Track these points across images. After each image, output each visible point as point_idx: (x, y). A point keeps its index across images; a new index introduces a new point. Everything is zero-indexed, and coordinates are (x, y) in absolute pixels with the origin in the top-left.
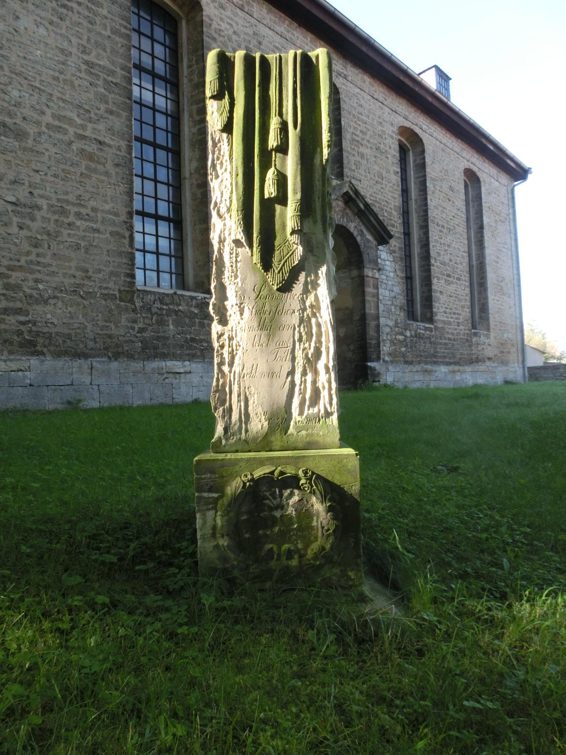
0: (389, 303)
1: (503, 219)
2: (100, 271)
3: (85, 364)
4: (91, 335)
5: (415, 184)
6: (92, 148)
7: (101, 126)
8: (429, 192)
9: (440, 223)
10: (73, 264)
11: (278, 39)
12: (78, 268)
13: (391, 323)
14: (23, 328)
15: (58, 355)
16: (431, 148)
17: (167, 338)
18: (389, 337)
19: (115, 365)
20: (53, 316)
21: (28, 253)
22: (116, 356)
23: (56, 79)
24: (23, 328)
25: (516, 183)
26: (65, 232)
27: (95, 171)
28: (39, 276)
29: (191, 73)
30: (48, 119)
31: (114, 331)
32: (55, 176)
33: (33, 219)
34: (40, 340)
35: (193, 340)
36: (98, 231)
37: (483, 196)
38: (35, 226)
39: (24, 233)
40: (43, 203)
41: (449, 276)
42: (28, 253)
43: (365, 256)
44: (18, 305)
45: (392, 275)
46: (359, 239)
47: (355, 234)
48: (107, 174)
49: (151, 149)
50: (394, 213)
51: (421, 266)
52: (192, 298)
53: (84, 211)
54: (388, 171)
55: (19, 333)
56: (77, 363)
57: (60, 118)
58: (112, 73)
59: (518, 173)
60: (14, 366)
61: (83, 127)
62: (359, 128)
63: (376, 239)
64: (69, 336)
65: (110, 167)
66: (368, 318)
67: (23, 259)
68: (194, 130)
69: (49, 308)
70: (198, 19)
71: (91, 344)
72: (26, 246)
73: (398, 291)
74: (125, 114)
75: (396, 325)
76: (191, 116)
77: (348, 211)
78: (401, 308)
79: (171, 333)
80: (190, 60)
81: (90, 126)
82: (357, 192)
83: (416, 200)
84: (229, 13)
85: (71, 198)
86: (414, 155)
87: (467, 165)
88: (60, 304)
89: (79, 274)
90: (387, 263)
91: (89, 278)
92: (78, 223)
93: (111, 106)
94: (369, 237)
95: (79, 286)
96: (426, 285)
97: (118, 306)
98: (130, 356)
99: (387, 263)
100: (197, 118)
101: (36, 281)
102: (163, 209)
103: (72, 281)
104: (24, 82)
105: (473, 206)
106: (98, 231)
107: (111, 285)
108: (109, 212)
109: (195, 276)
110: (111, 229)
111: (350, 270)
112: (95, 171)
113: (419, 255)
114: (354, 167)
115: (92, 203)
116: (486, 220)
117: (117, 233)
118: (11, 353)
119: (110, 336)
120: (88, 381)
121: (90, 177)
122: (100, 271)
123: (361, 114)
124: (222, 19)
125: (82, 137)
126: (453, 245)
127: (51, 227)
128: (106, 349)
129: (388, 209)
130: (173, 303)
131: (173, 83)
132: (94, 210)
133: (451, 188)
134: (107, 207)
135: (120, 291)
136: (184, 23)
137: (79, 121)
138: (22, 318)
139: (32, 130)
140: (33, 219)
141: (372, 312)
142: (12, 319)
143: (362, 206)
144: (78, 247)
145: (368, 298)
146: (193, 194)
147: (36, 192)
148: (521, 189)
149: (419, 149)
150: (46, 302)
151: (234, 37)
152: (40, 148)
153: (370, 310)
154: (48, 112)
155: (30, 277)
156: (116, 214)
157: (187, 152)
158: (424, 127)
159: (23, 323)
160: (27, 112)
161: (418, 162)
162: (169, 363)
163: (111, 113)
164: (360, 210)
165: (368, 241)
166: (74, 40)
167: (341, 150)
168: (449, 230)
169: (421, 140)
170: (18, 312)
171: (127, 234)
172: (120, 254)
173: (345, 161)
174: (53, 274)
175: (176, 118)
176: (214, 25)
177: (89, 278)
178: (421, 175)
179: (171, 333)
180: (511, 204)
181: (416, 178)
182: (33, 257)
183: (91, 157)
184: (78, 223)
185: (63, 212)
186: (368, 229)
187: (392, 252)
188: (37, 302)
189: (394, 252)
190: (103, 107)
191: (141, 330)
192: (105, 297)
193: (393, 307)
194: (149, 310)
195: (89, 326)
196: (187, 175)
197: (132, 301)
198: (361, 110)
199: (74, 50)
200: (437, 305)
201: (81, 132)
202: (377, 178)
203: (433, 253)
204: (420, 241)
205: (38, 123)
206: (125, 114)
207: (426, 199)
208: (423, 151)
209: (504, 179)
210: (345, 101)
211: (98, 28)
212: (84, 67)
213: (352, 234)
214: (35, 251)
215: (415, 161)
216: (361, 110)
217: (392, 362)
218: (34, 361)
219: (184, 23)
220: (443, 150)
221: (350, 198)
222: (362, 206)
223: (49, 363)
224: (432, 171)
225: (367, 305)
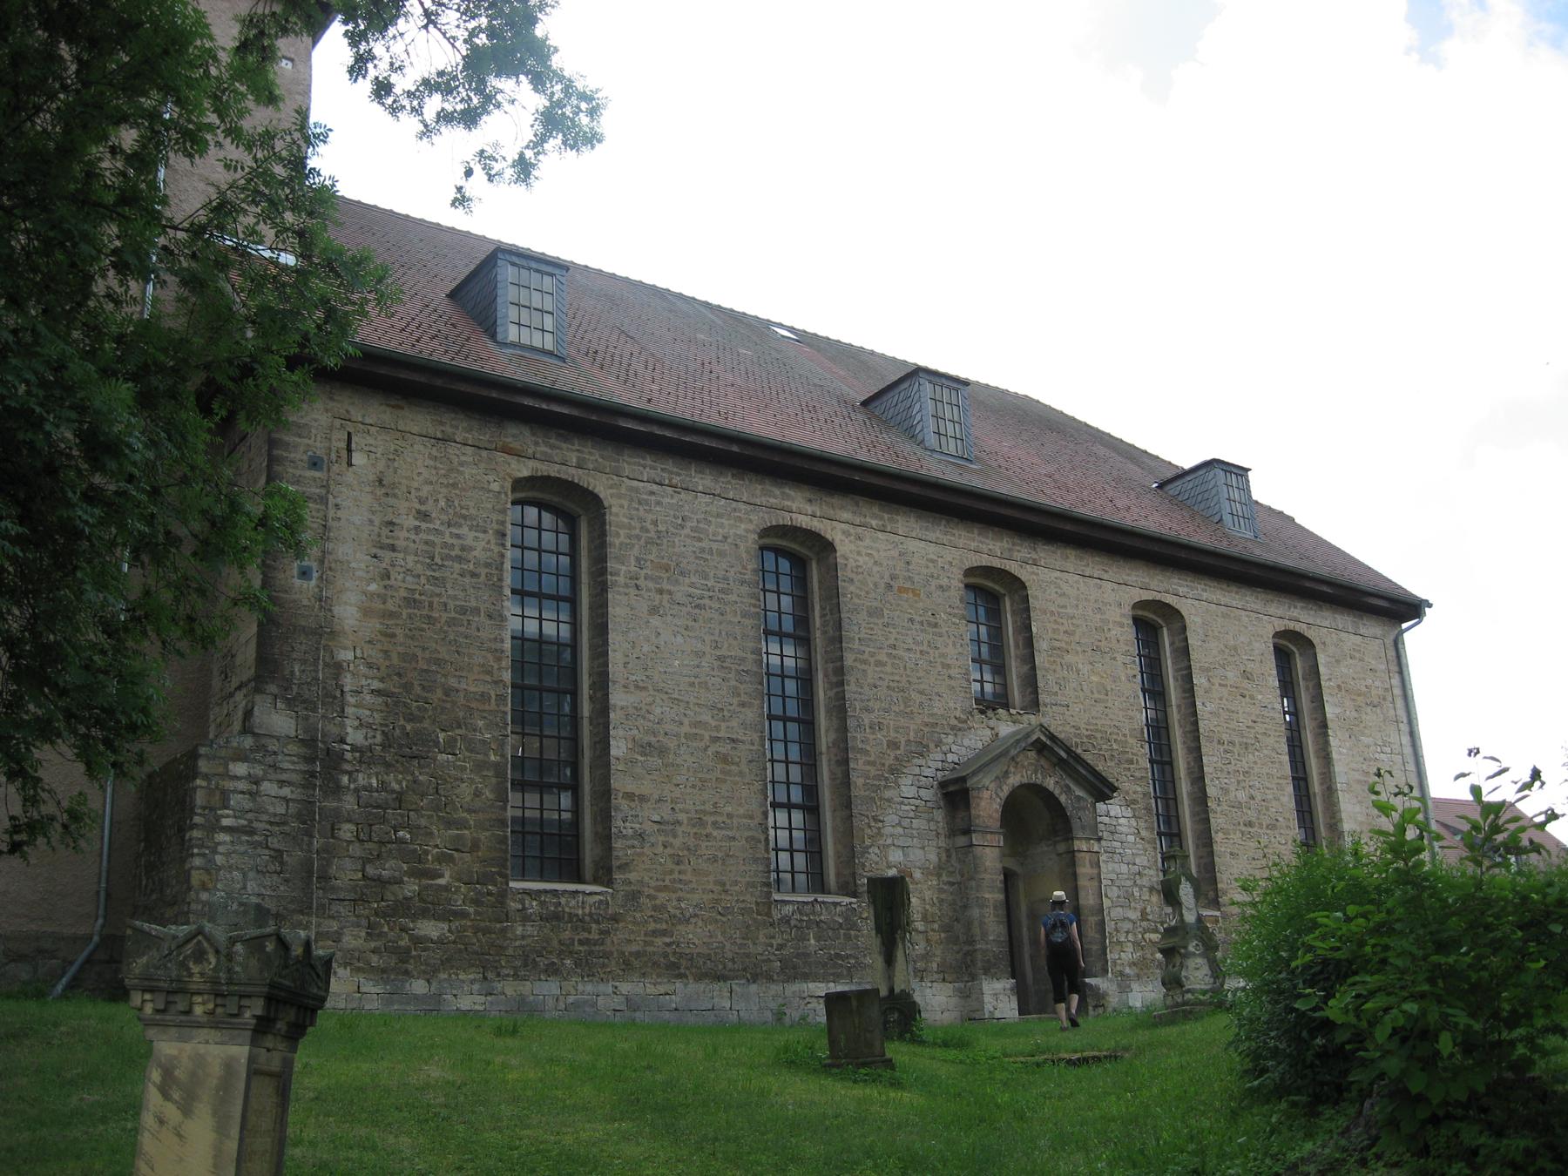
0: (1129, 883)
1: (1376, 701)
2: (736, 883)
3: (723, 987)
4: (729, 955)
5: (1176, 679)
6: (725, 748)
7: (734, 723)
8: (1198, 692)
9: (1225, 737)
10: (711, 878)
11: (932, 548)
12: (717, 882)
13: (1134, 915)
14: (668, 950)
15: (699, 977)
16: (1198, 620)
17: (809, 955)
18: (1130, 937)
19: (753, 988)
20: (694, 936)
21: (672, 872)
22: (754, 979)
23: (692, 684)
24: (668, 950)
25: (1404, 626)
26: (704, 845)
27: (729, 773)
28: (680, 894)
29: (825, 624)
30: (686, 729)
31: (752, 949)
32: (693, 787)
33: (675, 836)
34: (684, 962)
35: (838, 956)
36: (734, 838)
37: (1321, 669)
38: (677, 842)
39: (669, 851)
40: (682, 817)
41: (1250, 824)
42: (672, 872)
43: (1075, 824)
44: (664, 926)
45: (1131, 838)
46: (1063, 799)
47: (1057, 792)
48: (741, 773)
49: (772, 555)
50: (1131, 741)
51: (1193, 814)
52: (836, 904)
53: (720, 819)
54: (1115, 679)
55: (666, 955)
56: (717, 986)
57: (697, 724)
58: (743, 660)
59: (1407, 609)
60: (662, 989)
61: (717, 728)
62: (1062, 629)
63: (1091, 794)
64: (709, 957)
65: (744, 768)
66: (1084, 912)
67: (668, 878)
68: (831, 693)
69: (691, 927)
70: (831, 560)
71: (730, 965)
72: (670, 866)
73: (1145, 863)
74: (757, 702)
75: (1144, 914)
76: (826, 675)
77: (1043, 762)
78: (1151, 889)
79: (812, 949)
80: (822, 608)
81: (723, 725)
82: (1052, 737)
83: (1179, 706)
84: (867, 542)
85: (709, 807)
86: (1171, 634)
87: (1280, 625)
88: (700, 923)
89: (717, 888)
90: (1122, 821)
91: (726, 891)
92: (715, 833)
93: (744, 698)
94: (1079, 792)
95: (717, 901)
96: (1205, 845)
97: (755, 920)
98: (770, 979)
99: (1122, 821)
100: (834, 680)
101: (679, 900)
102: (797, 795)
103: (711, 896)
104: (665, 697)
105: (1307, 688)
106: (734, 838)
107: (748, 898)
108: (745, 816)
109: (838, 875)
110: (747, 834)
111: (1055, 843)
112: (729, 773)
113: (1189, 794)
114: (1056, 688)
115: (729, 809)
116: (1330, 711)
117: (753, 838)
118: (659, 976)
119: (748, 955)
120: (728, 1006)
121: (725, 781)
122: (736, 883)
123: (1064, 607)
124: (859, 553)
125: (716, 740)
126: (1256, 770)
127: (691, 842)
128: (745, 970)
129: (1120, 738)
130: (813, 913)
131: (802, 638)
132: (729, 816)
133: (1246, 675)
134: (742, 811)
135: (757, 904)
136: (814, 565)
137: (714, 723)
138: (668, 940)
139: (672, 745)
140: (675, 836)
141: (1091, 902)
142: (659, 941)
143: (1063, 754)
144: (715, 860)
145: (1082, 882)
146: (832, 773)
147: (678, 807)
148: (1416, 638)
149: (1178, 625)
150: (688, 921)
151: (876, 569)
152: (679, 761)
153: (1087, 899)
154: (686, 721)
155: (674, 896)
156: (751, 817)
157: (823, 720)
158: (1181, 590)
159: (668, 945)
160: (669, 727)
161: (1177, 644)
162: (811, 985)
163: (743, 705)
164: (1061, 759)
165: (1079, 798)
166: (707, 638)
167: (1034, 668)
168: (1246, 746)
169: (1178, 612)
170: (664, 933)
171: (762, 838)
172: (756, 860)
173: (1040, 684)
174: (693, 890)
175: (806, 679)
176: (851, 563)
177: (726, 891)
178: (1183, 665)
179: (812, 949)
180: (1394, 668)
181: (1177, 671)
182: (676, 876)
183: (725, 759)
184: (715, 833)
185: (701, 823)
186: (1077, 783)
187: (1129, 804)
188: (680, 922)
189: (1134, 802)
190: (735, 701)
191: (780, 947)
192: (743, 911)
193: (1136, 890)
194: (788, 922)
195: (728, 946)
196: (824, 749)
197: (769, 914)
198: (1062, 601)
199: (707, 650)
200: (1224, 877)
201: (715, 734)
202: (1096, 696)
203: (1211, 791)
204: (1190, 772)
205: (677, 735)
206: (757, 702)
207: (1194, 705)
208: (1184, 628)
209: (1372, 628)
210: (1036, 597)
211: (729, 617)
212: (716, 664)
213: (1051, 794)
214: (677, 868)
215: (1172, 644)
216: (1062, 601)
217: (1138, 976)
218: (679, 985)
219: (814, 565)
220: (1225, 616)
221: (1044, 745)
222: (1063, 754)
223: (693, 987)
224: (1199, 657)
225: (1082, 894)
